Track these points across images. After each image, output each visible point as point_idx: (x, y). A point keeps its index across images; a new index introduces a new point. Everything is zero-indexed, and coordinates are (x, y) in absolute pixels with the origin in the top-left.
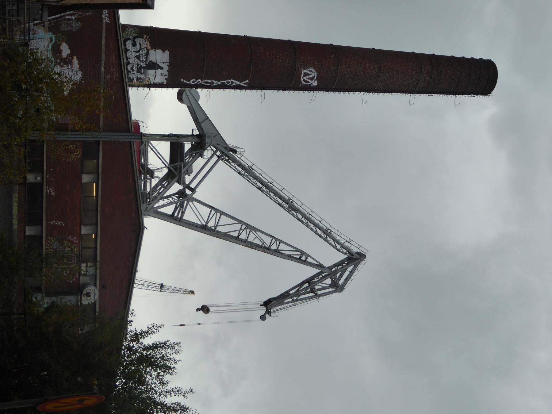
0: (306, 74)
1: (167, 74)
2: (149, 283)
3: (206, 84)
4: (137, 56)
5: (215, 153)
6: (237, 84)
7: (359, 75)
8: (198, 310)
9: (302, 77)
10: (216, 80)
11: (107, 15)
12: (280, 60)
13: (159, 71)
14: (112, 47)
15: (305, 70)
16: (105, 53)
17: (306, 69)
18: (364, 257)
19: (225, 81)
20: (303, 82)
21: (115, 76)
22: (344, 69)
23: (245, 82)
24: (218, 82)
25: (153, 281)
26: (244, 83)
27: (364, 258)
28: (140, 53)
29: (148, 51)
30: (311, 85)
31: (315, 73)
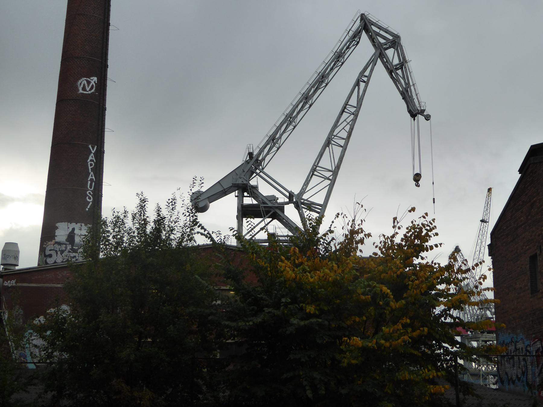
0: (84, 89)
1: (80, 224)
2: (480, 234)
3: (93, 186)
4: (60, 253)
5: (258, 174)
6: (93, 156)
7: (86, 36)
8: (418, 185)
9: (87, 93)
10: (88, 177)
11: (9, 282)
12: (69, 114)
13: (77, 231)
14: (39, 277)
15: (79, 90)
16: (44, 284)
17: (78, 89)
18: (363, 16)
19: (90, 168)
20: (93, 91)
21: (66, 274)
22: (79, 51)
23: (91, 148)
24: (91, 174)
25: (478, 229)
26: (92, 149)
27: (364, 16)
28: (58, 250)
29: (56, 243)
30: (96, 82)
31: (83, 80)
